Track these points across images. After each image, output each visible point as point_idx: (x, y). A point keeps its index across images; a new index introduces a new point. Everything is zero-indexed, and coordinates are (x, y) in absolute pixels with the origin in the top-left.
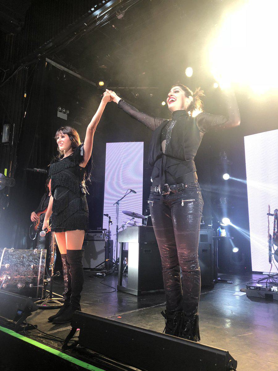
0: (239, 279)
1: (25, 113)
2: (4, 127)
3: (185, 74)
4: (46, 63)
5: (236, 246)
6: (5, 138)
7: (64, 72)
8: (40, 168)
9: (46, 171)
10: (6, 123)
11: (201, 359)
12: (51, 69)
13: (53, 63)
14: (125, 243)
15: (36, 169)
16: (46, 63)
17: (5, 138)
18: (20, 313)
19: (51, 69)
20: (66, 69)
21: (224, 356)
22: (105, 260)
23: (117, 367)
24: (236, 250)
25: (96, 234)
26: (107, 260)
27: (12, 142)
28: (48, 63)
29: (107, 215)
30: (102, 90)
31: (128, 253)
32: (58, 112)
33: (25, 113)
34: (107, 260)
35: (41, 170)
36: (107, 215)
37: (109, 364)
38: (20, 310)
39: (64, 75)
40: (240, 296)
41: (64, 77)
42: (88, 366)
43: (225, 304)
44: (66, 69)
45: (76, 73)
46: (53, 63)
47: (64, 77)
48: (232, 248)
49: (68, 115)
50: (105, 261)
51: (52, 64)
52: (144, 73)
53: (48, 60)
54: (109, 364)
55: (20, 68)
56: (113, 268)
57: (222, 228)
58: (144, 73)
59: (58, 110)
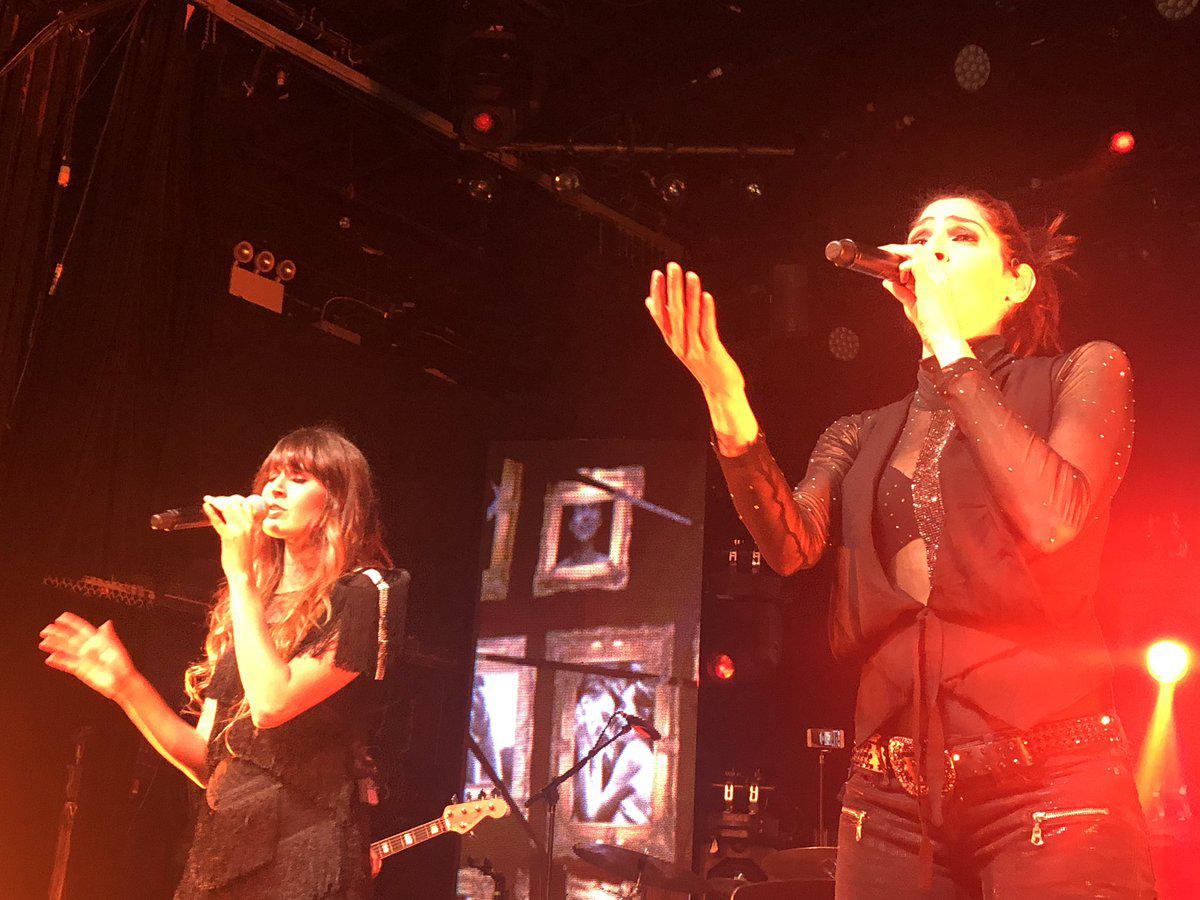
1: (59, 271)
3: (931, 201)
4: (190, 9)
7: (282, 57)
9: (152, 596)
15: (92, 581)
16: (190, 9)
20: (294, 45)
23: (1059, 815)
30: (841, 761)
32: (236, 270)
33: (59, 271)
35: (120, 588)
37: (1073, 813)
39: (282, 74)
41: (280, 82)
44: (294, 45)
45: (348, 63)
47: (280, 82)
49: (290, 286)
52: (718, 72)
54: (1073, 813)
55: (49, 34)
58: (718, 72)
59: (232, 259)
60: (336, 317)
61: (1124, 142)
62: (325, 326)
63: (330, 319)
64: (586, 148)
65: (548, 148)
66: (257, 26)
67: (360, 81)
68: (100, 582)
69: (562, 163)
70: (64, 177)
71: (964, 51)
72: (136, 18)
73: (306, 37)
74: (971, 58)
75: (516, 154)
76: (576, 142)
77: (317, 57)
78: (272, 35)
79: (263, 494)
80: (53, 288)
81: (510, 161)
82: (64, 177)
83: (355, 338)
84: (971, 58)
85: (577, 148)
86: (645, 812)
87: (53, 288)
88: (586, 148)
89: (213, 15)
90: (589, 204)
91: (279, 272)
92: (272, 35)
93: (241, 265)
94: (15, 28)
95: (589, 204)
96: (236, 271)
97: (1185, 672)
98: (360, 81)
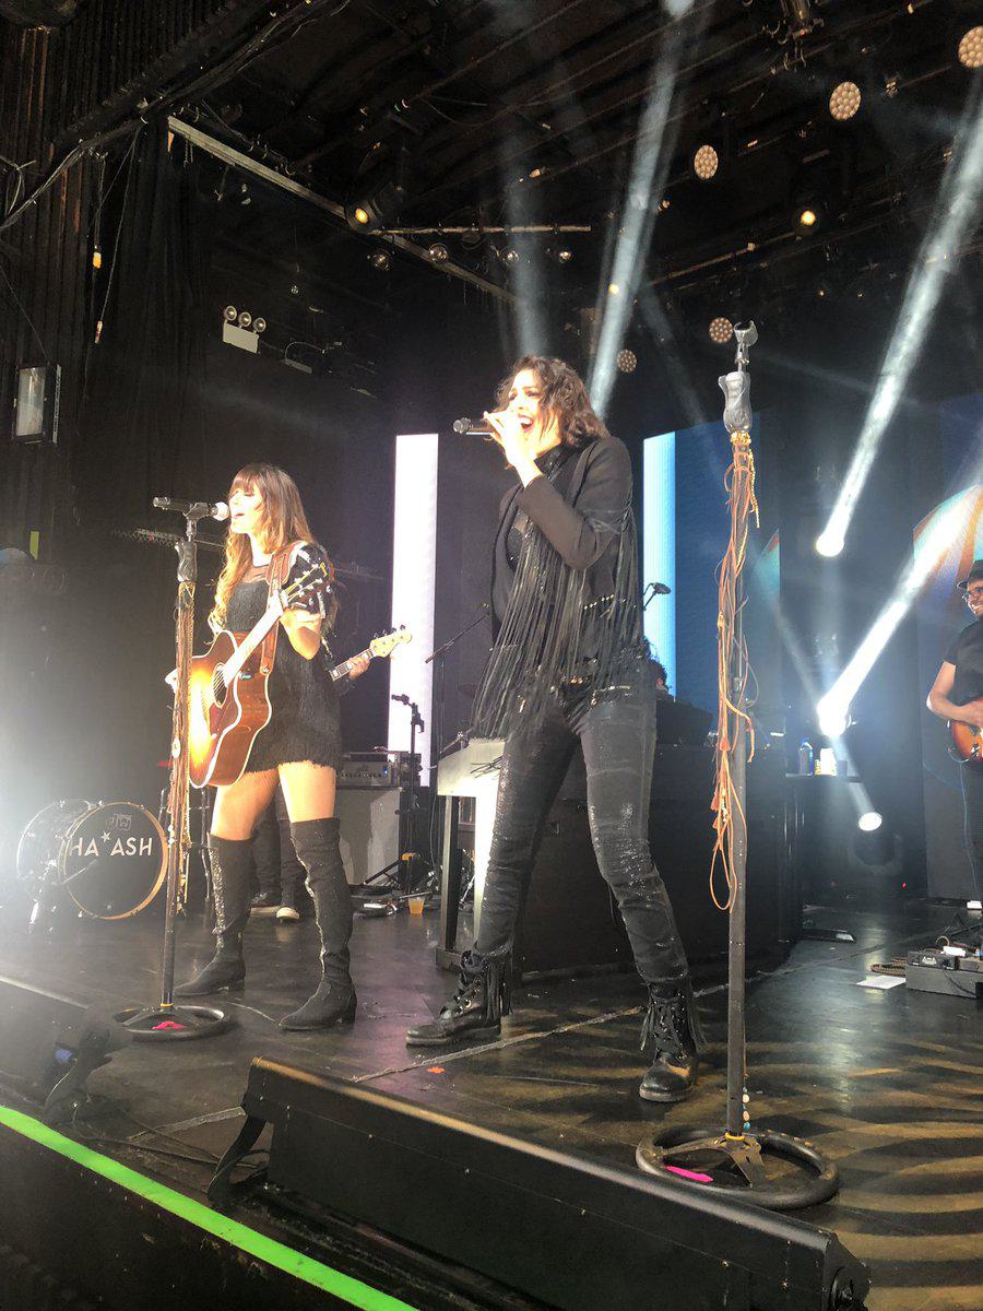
0: (881, 925)
1: (100, 326)
2: (23, 377)
4: (171, 136)
5: (877, 807)
6: (29, 418)
7: (238, 173)
8: (160, 530)
10: (28, 364)
11: (727, 1260)
12: (189, 160)
13: (198, 138)
14: (455, 799)
15: (143, 532)
16: (171, 136)
17: (29, 418)
18: (64, 1055)
19: (189, 160)
21: (820, 1252)
22: (400, 857)
24: (870, 822)
25: (367, 764)
26: (406, 857)
27: (55, 434)
28: (179, 138)
29: (405, 699)
31: (473, 833)
33: (100, 326)
34: (406, 857)
36: (405, 699)
38: (65, 1047)
40: (883, 990)
42: (300, 1263)
43: (831, 1021)
45: (287, 176)
46: (198, 138)
48: (855, 816)
49: (263, 336)
50: (400, 862)
51: (192, 139)
53: (175, 123)
55: (74, 157)
56: (429, 884)
57: (841, 1091)
60: (295, 356)
61: (808, 218)
62: (288, 362)
63: (291, 358)
64: (451, 230)
65: (425, 231)
66: (221, 149)
67: (293, 186)
68: (148, 533)
69: (433, 240)
70: (97, 260)
71: (701, 151)
72: (134, 143)
73: (255, 156)
74: (705, 155)
75: (405, 236)
76: (443, 227)
77: (265, 172)
78: (232, 156)
79: (395, 623)
80: (97, 338)
81: (401, 242)
82: (97, 260)
83: (308, 370)
84: (705, 155)
85: (445, 230)
86: (401, 853)
87: (97, 338)
88: (451, 230)
89: (190, 142)
90: (455, 269)
91: (255, 326)
92: (232, 156)
93: (229, 322)
94: (52, 154)
95: (455, 269)
96: (227, 328)
97: (933, 520)
98: (293, 186)
